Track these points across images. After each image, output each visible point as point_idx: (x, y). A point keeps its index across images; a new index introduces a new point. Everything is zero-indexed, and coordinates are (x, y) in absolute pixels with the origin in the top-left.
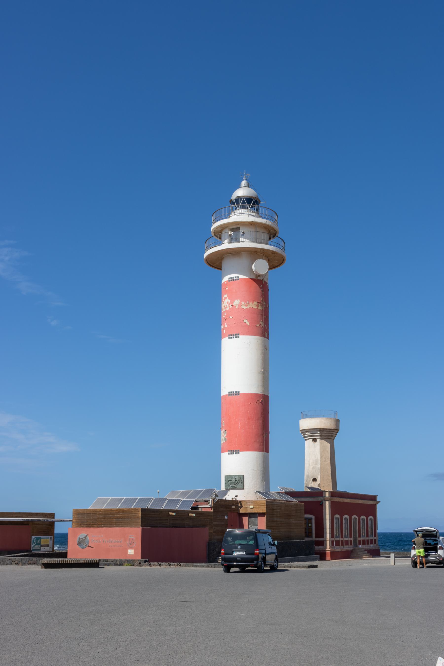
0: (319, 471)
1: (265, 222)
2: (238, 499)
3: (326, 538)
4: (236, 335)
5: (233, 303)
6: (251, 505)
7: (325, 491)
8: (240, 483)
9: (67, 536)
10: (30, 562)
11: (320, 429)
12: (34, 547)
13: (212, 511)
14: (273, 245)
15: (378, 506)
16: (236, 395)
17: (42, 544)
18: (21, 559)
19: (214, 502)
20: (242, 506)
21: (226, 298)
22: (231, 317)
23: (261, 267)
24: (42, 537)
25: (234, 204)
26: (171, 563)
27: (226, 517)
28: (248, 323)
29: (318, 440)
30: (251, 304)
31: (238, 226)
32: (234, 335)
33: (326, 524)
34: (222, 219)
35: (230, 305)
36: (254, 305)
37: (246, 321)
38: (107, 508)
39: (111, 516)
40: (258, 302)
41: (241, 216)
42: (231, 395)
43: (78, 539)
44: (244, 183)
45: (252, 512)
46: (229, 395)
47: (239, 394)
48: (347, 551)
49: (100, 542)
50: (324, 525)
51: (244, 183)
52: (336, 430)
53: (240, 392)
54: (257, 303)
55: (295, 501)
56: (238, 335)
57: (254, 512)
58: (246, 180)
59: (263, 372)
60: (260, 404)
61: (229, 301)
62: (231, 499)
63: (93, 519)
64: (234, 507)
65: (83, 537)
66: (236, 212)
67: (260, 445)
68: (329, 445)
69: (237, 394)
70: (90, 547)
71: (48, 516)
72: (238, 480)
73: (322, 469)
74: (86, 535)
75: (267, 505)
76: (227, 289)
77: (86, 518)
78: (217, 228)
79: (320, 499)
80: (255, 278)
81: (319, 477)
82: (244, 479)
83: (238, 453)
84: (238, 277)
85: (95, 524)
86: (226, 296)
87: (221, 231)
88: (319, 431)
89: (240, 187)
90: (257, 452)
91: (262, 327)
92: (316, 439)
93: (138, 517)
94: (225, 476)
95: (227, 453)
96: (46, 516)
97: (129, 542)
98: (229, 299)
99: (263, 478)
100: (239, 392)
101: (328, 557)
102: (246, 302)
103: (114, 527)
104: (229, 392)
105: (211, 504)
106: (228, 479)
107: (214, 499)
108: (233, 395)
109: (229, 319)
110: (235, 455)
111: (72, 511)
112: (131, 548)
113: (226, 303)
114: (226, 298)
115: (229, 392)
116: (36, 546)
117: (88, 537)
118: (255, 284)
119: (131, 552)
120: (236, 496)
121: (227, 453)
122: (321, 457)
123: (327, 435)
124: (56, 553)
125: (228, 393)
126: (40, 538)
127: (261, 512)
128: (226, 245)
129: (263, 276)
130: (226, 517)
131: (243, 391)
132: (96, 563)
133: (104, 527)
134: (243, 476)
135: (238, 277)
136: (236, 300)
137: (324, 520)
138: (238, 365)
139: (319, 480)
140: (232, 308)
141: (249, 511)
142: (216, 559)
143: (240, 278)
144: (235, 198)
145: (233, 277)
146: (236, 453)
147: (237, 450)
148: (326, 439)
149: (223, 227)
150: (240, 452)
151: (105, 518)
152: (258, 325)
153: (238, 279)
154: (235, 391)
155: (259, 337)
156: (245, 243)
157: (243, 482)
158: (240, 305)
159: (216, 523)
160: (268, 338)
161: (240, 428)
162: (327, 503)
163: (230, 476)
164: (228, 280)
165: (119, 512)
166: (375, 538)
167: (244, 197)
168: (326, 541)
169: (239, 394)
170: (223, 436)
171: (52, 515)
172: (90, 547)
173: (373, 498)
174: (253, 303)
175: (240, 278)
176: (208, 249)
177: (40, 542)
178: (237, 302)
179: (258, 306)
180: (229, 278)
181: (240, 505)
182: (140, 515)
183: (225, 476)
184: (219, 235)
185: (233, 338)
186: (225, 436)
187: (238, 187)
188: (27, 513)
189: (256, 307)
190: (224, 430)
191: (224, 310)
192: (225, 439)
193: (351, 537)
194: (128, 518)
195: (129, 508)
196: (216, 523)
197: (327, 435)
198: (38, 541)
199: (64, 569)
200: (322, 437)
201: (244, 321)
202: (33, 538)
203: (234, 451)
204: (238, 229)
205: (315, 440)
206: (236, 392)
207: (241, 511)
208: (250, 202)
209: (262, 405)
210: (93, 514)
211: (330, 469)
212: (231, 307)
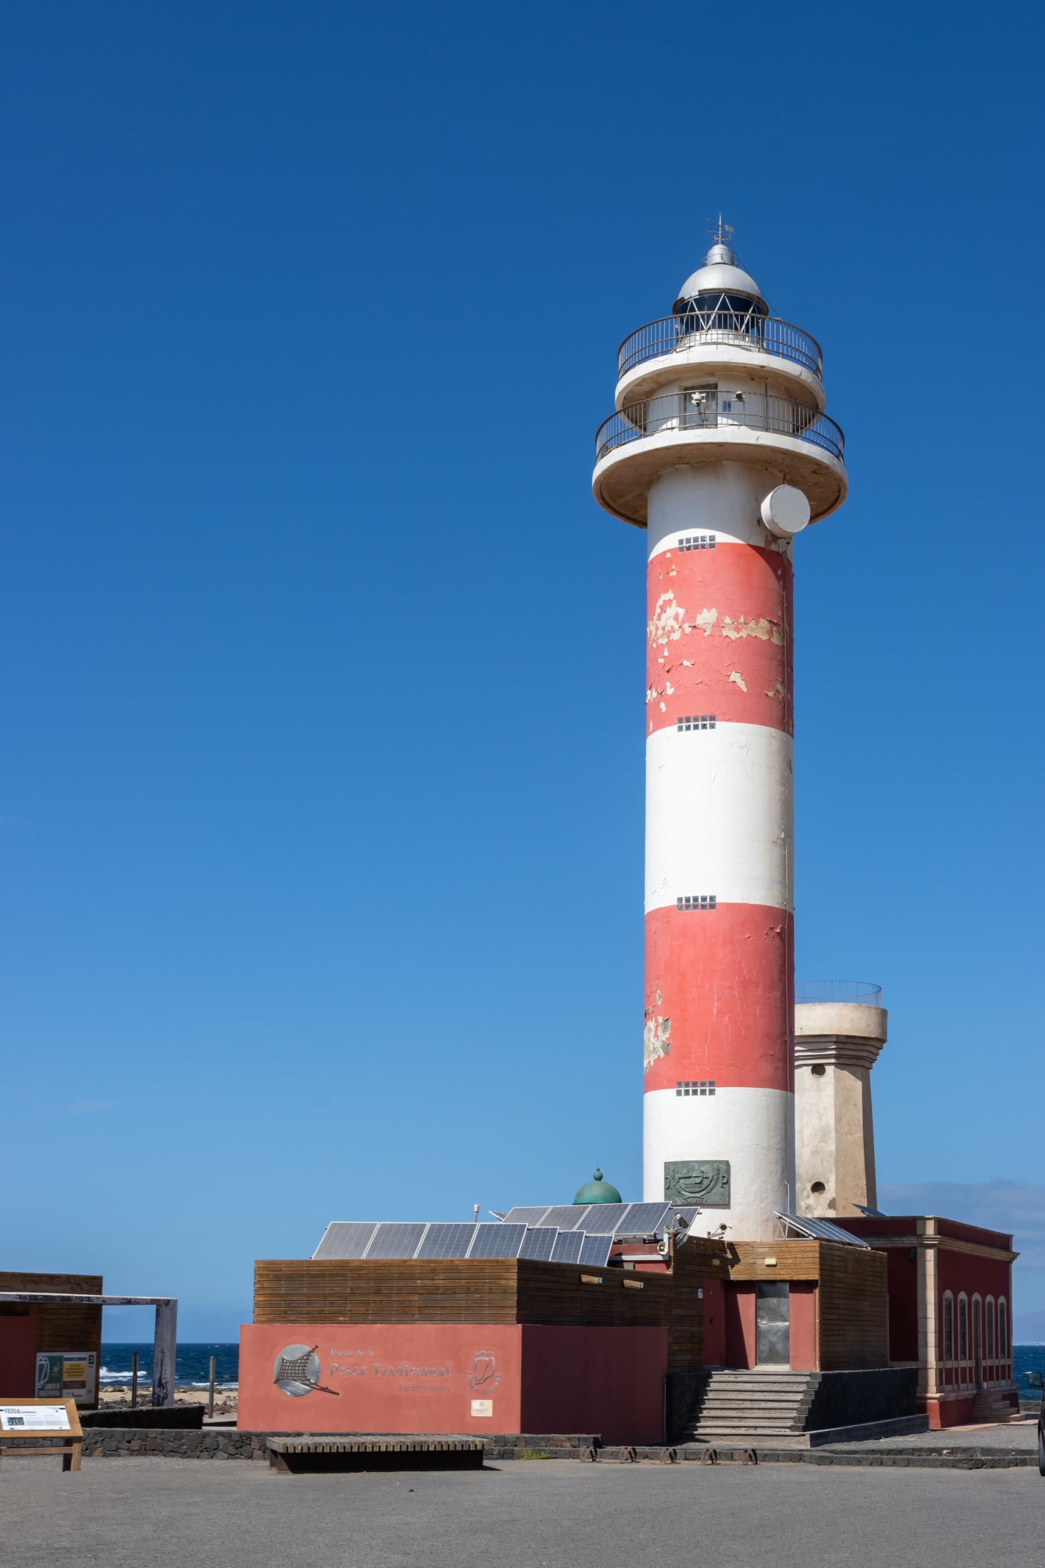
0: (832, 1161)
1: (797, 373)
2: (728, 1237)
3: (926, 1362)
4: (704, 719)
6: (770, 1256)
7: (924, 1219)
8: (718, 1187)
9: (238, 1351)
10: (136, 1444)
11: (837, 1036)
12: (42, 1389)
13: (670, 1272)
14: (822, 447)
15: (1015, 1265)
16: (704, 907)
17: (66, 1379)
18: (100, 1433)
19: (675, 1245)
20: (736, 1260)
21: (668, 603)
22: (686, 663)
24: (67, 1355)
25: (692, 309)
26: (639, 1449)
27: (700, 1295)
28: (742, 685)
29: (830, 1070)
30: (752, 624)
31: (712, 380)
32: (688, 721)
33: (926, 1318)
34: (640, 362)
35: (686, 626)
36: (760, 630)
37: (735, 677)
38: (321, 1258)
39: (402, 1284)
40: (770, 622)
41: (710, 347)
42: (688, 907)
43: (277, 1363)
44: (717, 252)
45: (771, 1277)
46: (680, 907)
47: (713, 906)
48: (966, 1400)
49: (362, 1373)
50: (920, 1322)
51: (717, 252)
52: (882, 1041)
54: (767, 625)
55: (864, 1246)
56: (713, 718)
57: (778, 1277)
58: (723, 243)
59: (783, 840)
60: (777, 939)
61: (681, 612)
62: (705, 1236)
63: (331, 1295)
64: (716, 1262)
65: (299, 1355)
66: (697, 337)
67: (776, 1069)
68: (859, 1084)
69: (709, 904)
70: (322, 1389)
71: (85, 1286)
72: (710, 1175)
73: (841, 1157)
74: (307, 1349)
75: (823, 1257)
76: (673, 574)
77: (305, 1291)
79: (907, 1241)
80: (762, 544)
81: (832, 1178)
82: (729, 1174)
83: (712, 1092)
84: (712, 538)
85: (339, 1313)
86: (669, 595)
87: (650, 394)
88: (836, 1042)
89: (704, 265)
90: (768, 1090)
92: (822, 1066)
93: (505, 1291)
94: (667, 1165)
95: (674, 1091)
96: (79, 1285)
97: (478, 1378)
98: (679, 605)
99: (783, 1171)
100: (712, 898)
101: (935, 1421)
102: (735, 618)
103: (414, 1322)
104: (680, 900)
105: (666, 1250)
106: (675, 1173)
107: (675, 1235)
109: (680, 669)
110: (691, 1097)
111: (252, 1267)
112: (483, 1396)
113: (667, 619)
114: (668, 603)
115: (680, 900)
116: (49, 1386)
117: (316, 1359)
118: (761, 564)
119: (481, 1408)
120: (723, 1227)
121: (674, 1091)
122: (839, 1119)
123: (855, 1054)
124: (170, 1410)
125: (675, 903)
126: (61, 1360)
127: (803, 1277)
128: (669, 436)
129: (788, 538)
130: (700, 1295)
131: (729, 893)
132: (476, 1451)
133: (375, 1322)
134: (727, 1163)
135: (712, 538)
136: (705, 611)
137: (919, 1306)
138: (705, 810)
139: (831, 1190)
140: (691, 634)
141: (762, 1275)
142: (686, 1428)
144: (695, 294)
145: (690, 538)
146: (703, 1092)
147: (707, 1081)
148: (852, 1068)
149: (661, 380)
150: (718, 1090)
151: (378, 1292)
152: (771, 694)
153: (712, 546)
154: (691, 895)
156: (728, 431)
157: (728, 1182)
158: (718, 625)
159: (679, 1312)
160: (792, 736)
161: (718, 1012)
162: (930, 1254)
163: (685, 1164)
164: (676, 545)
165: (434, 1270)
166: (1008, 1362)
167: (726, 291)
168: (925, 1369)
169: (713, 906)
170: (655, 1039)
171: (95, 1283)
172: (322, 1389)
173: (1003, 1242)
174: (757, 622)
176: (606, 450)
177: (60, 1372)
178: (707, 617)
179: (770, 632)
180: (681, 542)
181: (729, 1256)
182: (514, 1283)
183: (667, 1165)
184: (638, 412)
185: (696, 727)
186: (665, 1036)
187: (700, 262)
188: (24, 1275)
189: (765, 637)
190: (660, 1019)
192: (666, 1046)
193: (970, 1358)
194: (468, 1291)
195: (405, 1258)
196: (679, 1312)
197: (855, 1054)
198: (56, 1370)
199: (365, 1475)
200: (841, 1061)
201: (732, 678)
202: (42, 1358)
203: (696, 1083)
204: (711, 390)
205: (818, 1070)
207: (736, 1274)
208: (737, 310)
209: (776, 947)
210: (331, 1276)
211: (863, 1158)
212: (688, 630)
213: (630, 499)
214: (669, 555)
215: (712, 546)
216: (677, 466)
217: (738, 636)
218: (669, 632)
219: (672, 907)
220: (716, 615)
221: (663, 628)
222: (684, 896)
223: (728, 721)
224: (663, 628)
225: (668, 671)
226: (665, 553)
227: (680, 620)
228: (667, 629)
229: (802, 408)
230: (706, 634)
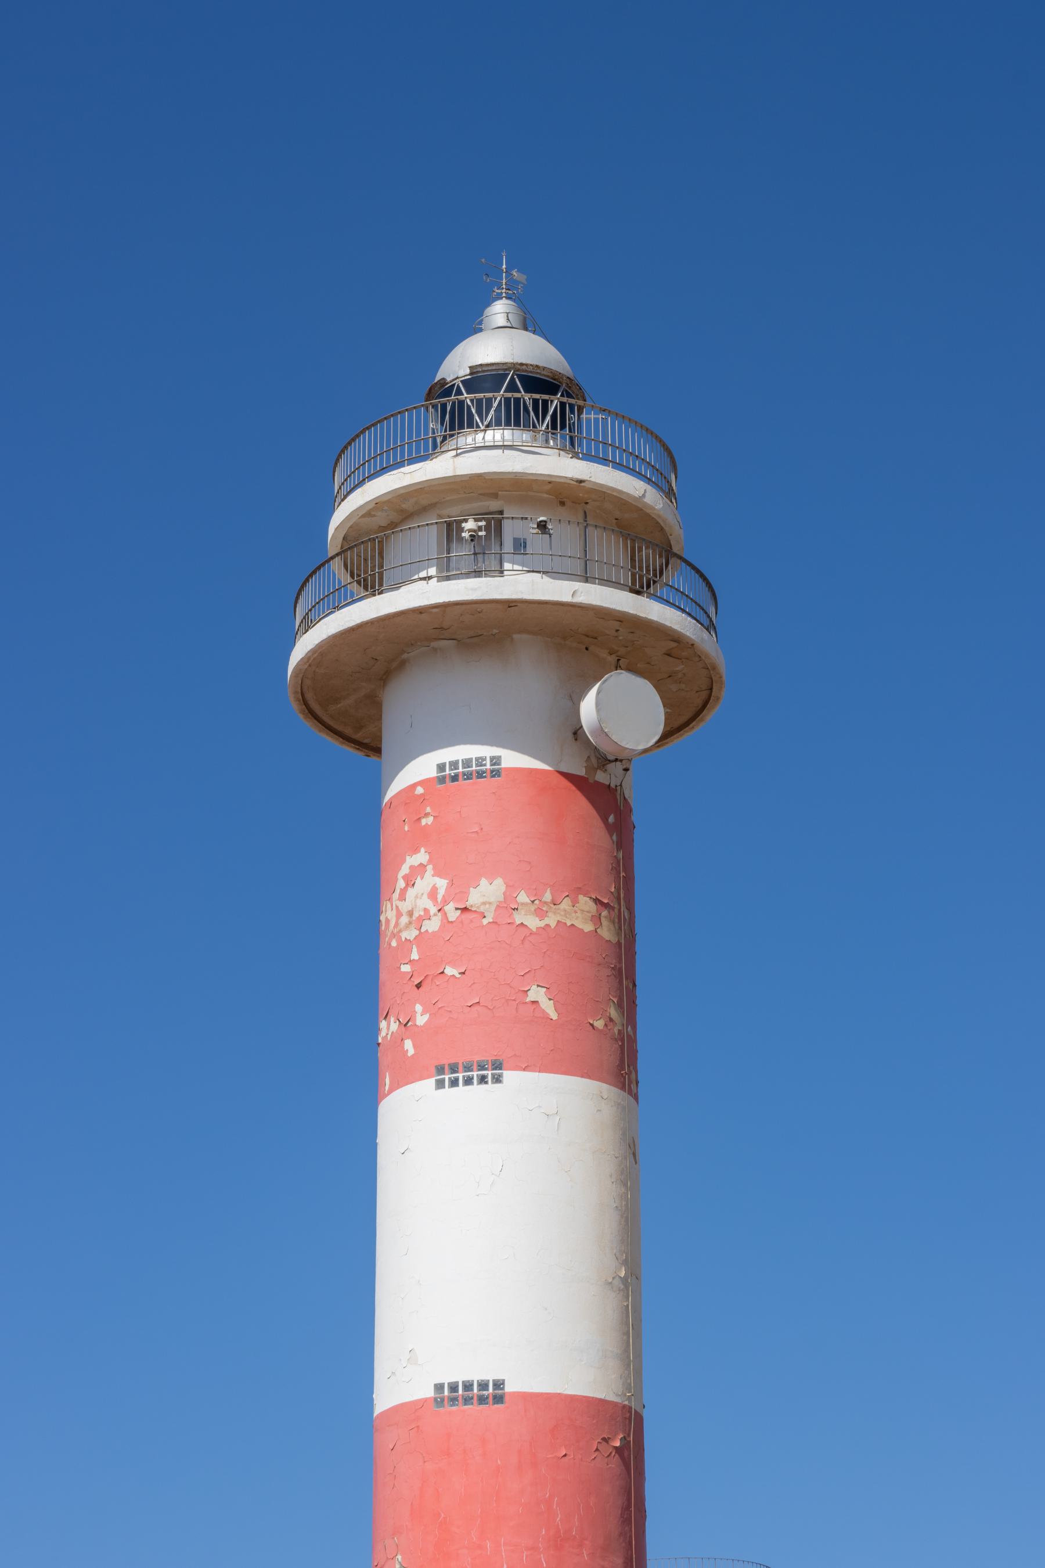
1: (638, 494)
4: (482, 1067)
5: (465, 894)
16: (482, 1400)
22: (450, 971)
23: (620, 710)
28: (548, 1007)
30: (566, 904)
35: (450, 908)
36: (579, 914)
37: (537, 994)
40: (597, 901)
46: (439, 1402)
47: (499, 1399)
51: (499, 311)
53: (509, 1388)
54: (592, 907)
56: (498, 1065)
60: (616, 1459)
61: (442, 884)
66: (468, 439)
69: (492, 1394)
78: (378, 505)
80: (582, 772)
84: (496, 760)
86: (421, 857)
89: (481, 330)
91: (617, 1038)
98: (437, 873)
100: (499, 1384)
102: (536, 896)
104: (439, 1387)
108: (467, 1400)
113: (416, 899)
115: (439, 1387)
118: (581, 804)
125: (430, 1393)
128: (422, 592)
129: (623, 760)
135: (496, 760)
136: (484, 882)
143: (504, 764)
144: (464, 372)
145: (458, 767)
149: (408, 506)
152: (599, 1024)
155: (605, 1086)
158: (508, 906)
164: (433, 773)
167: (516, 367)
169: (499, 1399)
175: (504, 764)
176: (308, 624)
178: (486, 893)
179: (597, 919)
180: (441, 767)
184: (367, 561)
185: (468, 1081)
187: (472, 325)
189: (588, 927)
191: (411, 934)
201: (532, 996)
206: (483, 1385)
208: (535, 398)
212: (453, 915)
213: (351, 705)
214: (420, 790)
215: (496, 773)
216: (434, 644)
217: (542, 924)
218: (421, 919)
219: (426, 1400)
220: (503, 888)
221: (410, 913)
222: (447, 1379)
223: (524, 1070)
224: (410, 913)
225: (418, 986)
226: (413, 786)
227: (440, 897)
228: (416, 915)
229: (646, 551)
230: (485, 922)
